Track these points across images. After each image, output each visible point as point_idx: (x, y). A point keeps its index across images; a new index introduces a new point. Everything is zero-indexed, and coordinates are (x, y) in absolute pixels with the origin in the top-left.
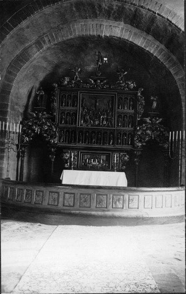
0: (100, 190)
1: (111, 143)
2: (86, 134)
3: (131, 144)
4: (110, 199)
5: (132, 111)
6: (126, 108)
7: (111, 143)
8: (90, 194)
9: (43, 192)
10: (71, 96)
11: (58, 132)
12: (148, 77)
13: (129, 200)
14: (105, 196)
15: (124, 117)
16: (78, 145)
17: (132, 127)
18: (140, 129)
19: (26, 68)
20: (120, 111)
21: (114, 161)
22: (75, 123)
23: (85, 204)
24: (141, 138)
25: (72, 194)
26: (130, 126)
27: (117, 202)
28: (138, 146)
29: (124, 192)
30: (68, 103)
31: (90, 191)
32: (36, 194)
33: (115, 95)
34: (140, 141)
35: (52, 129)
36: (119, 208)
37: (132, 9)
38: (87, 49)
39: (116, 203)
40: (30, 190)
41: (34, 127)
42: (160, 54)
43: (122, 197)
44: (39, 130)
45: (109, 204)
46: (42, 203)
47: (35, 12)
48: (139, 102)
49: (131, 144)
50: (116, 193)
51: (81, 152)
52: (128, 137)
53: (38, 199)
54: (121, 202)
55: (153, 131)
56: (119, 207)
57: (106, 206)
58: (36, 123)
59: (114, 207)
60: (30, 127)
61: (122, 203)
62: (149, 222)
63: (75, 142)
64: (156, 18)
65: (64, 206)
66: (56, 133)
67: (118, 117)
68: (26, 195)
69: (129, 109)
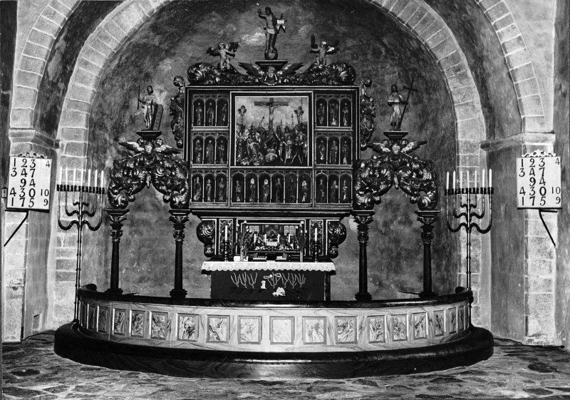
1: (304, 199)
2: (249, 180)
5: (347, 129)
7: (304, 199)
10: (214, 102)
11: (188, 181)
12: (381, 53)
15: (330, 143)
16: (294, 206)
17: (349, 163)
18: (367, 166)
19: (117, 53)
20: (321, 129)
21: (223, 234)
22: (225, 160)
30: (208, 116)
32: (153, 319)
35: (118, 179)
42: (403, 8)
52: (342, 186)
58: (142, 163)
63: (289, 200)
65: (208, 341)
67: (318, 141)
68: (133, 322)
69: (342, 125)
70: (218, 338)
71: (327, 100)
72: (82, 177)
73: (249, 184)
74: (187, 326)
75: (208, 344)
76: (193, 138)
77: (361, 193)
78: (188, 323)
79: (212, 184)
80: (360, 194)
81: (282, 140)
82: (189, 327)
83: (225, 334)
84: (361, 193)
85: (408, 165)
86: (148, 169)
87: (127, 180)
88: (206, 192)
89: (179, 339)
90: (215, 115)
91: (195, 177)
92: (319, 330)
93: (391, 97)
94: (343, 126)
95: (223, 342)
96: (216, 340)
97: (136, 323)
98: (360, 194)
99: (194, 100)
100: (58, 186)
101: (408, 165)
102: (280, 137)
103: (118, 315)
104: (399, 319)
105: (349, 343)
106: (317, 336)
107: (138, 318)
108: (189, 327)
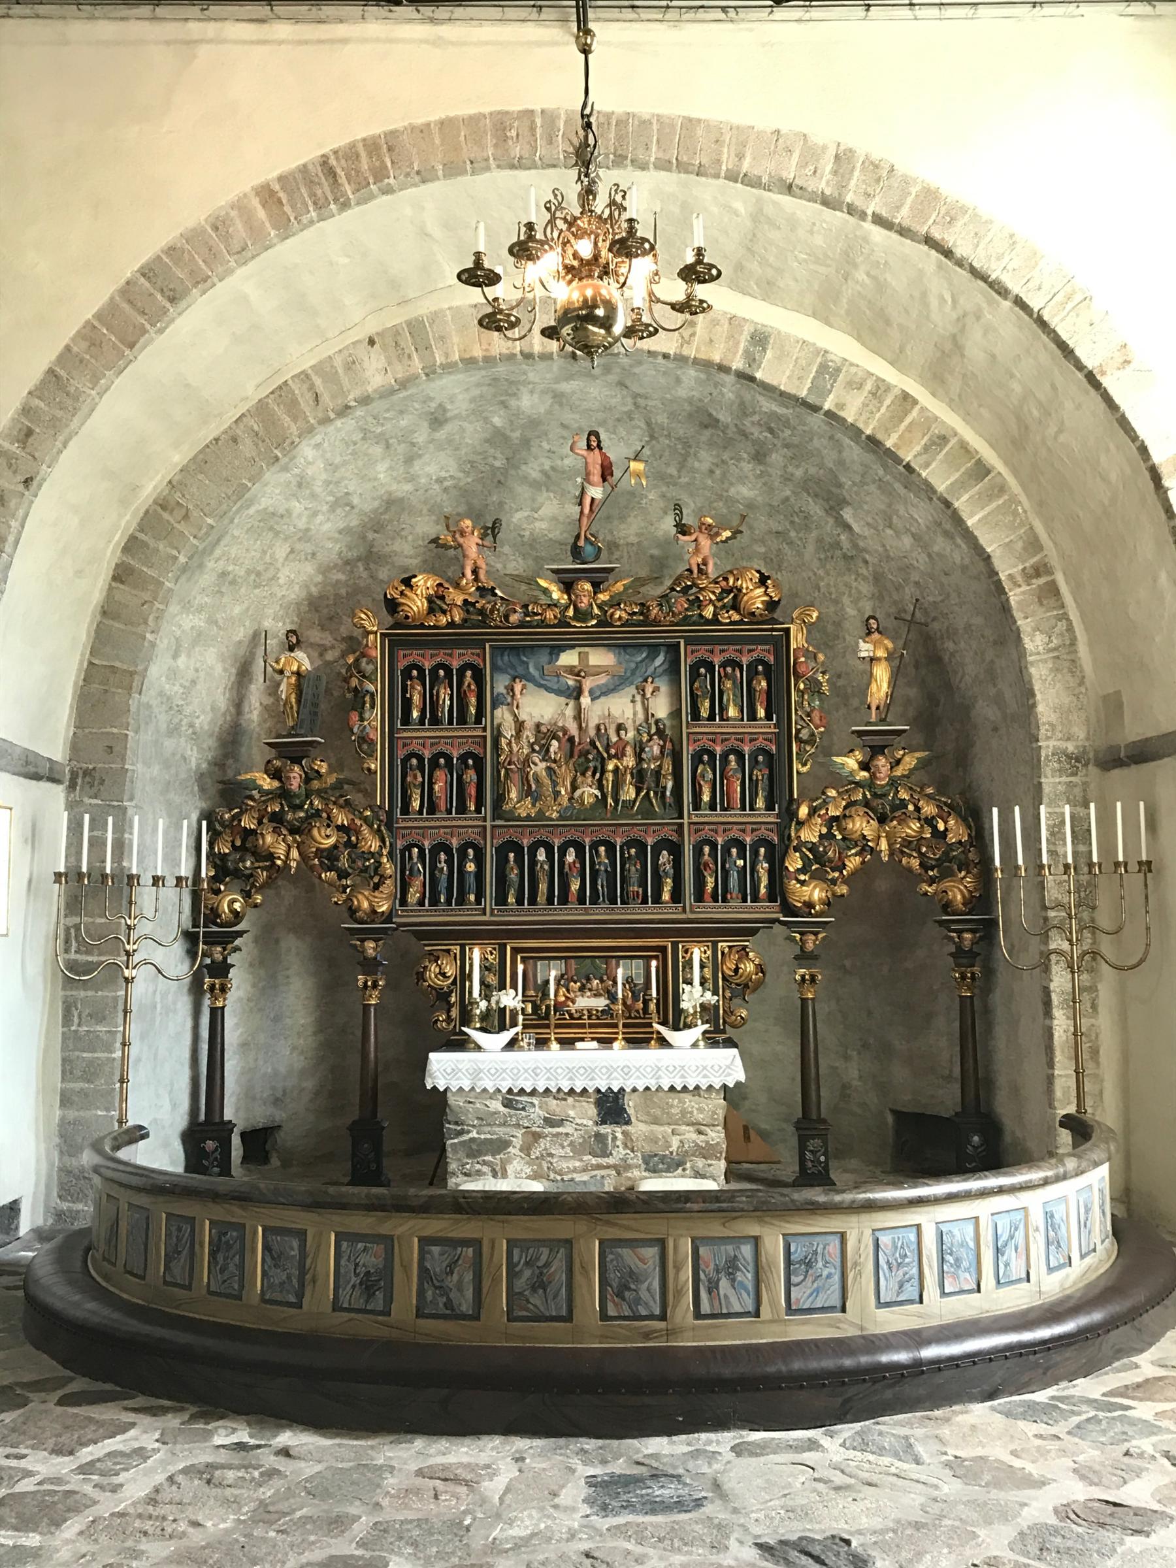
0: (625, 1219)
2: (563, 854)
3: (771, 898)
4: (678, 1268)
6: (732, 712)
8: (568, 1243)
9: (302, 1234)
13: (788, 1262)
14: (651, 1253)
17: (770, 807)
18: (813, 811)
23: (536, 1300)
24: (819, 858)
25: (465, 1243)
26: (760, 803)
27: (724, 1284)
28: (809, 905)
29: (761, 1221)
31: (561, 1227)
33: (202, 540)
34: (819, 876)
36: (729, 1315)
37: (739, 206)
38: (843, 1445)
39: (713, 1287)
40: (233, 1225)
41: (269, 839)
43: (747, 1250)
44: (295, 854)
45: (679, 1293)
46: (300, 1295)
47: (527, 533)
48: (798, 677)
49: (771, 898)
50: (715, 1229)
51: (515, 951)
53: (279, 1276)
54: (746, 1277)
55: (882, 820)
56: (737, 1308)
57: (657, 1312)
59: (705, 1308)
60: (247, 842)
61: (750, 1286)
62: (908, 1389)
64: (866, 239)
66: (379, 864)
68: (213, 1254)
70: (449, 1304)
71: (717, 661)
72: (948, 482)
73: (533, 862)
74: (361, 1270)
75: (421, 1321)
76: (401, 754)
77: (802, 877)
78: (362, 1259)
79: (449, 862)
80: (799, 881)
81: (610, 757)
82: (368, 1273)
83: (469, 1293)
84: (802, 877)
85: (911, 807)
86: (293, 831)
87: (243, 860)
88: (434, 881)
89: (336, 1307)
90: (451, 699)
91: (408, 848)
92: (739, 1277)
93: (863, 646)
94: (755, 719)
95: (464, 1317)
96: (442, 1310)
97: (220, 1257)
98: (803, 883)
99: (401, 665)
100: (514, 986)
101: (911, 807)
102: (607, 752)
103: (174, 1229)
104: (956, 1232)
105: (823, 1309)
106: (731, 1293)
107: (227, 1242)
108: (368, 1273)
